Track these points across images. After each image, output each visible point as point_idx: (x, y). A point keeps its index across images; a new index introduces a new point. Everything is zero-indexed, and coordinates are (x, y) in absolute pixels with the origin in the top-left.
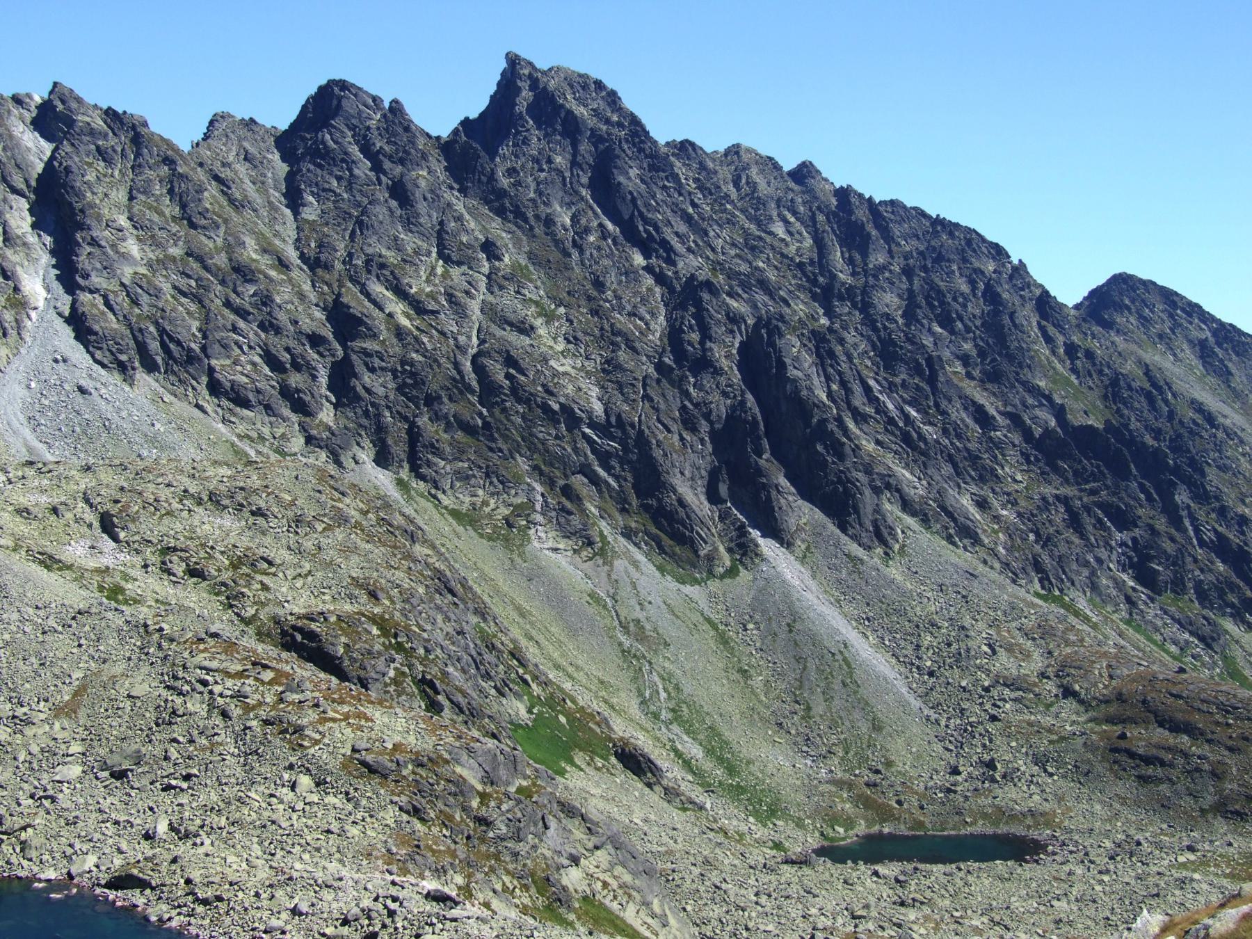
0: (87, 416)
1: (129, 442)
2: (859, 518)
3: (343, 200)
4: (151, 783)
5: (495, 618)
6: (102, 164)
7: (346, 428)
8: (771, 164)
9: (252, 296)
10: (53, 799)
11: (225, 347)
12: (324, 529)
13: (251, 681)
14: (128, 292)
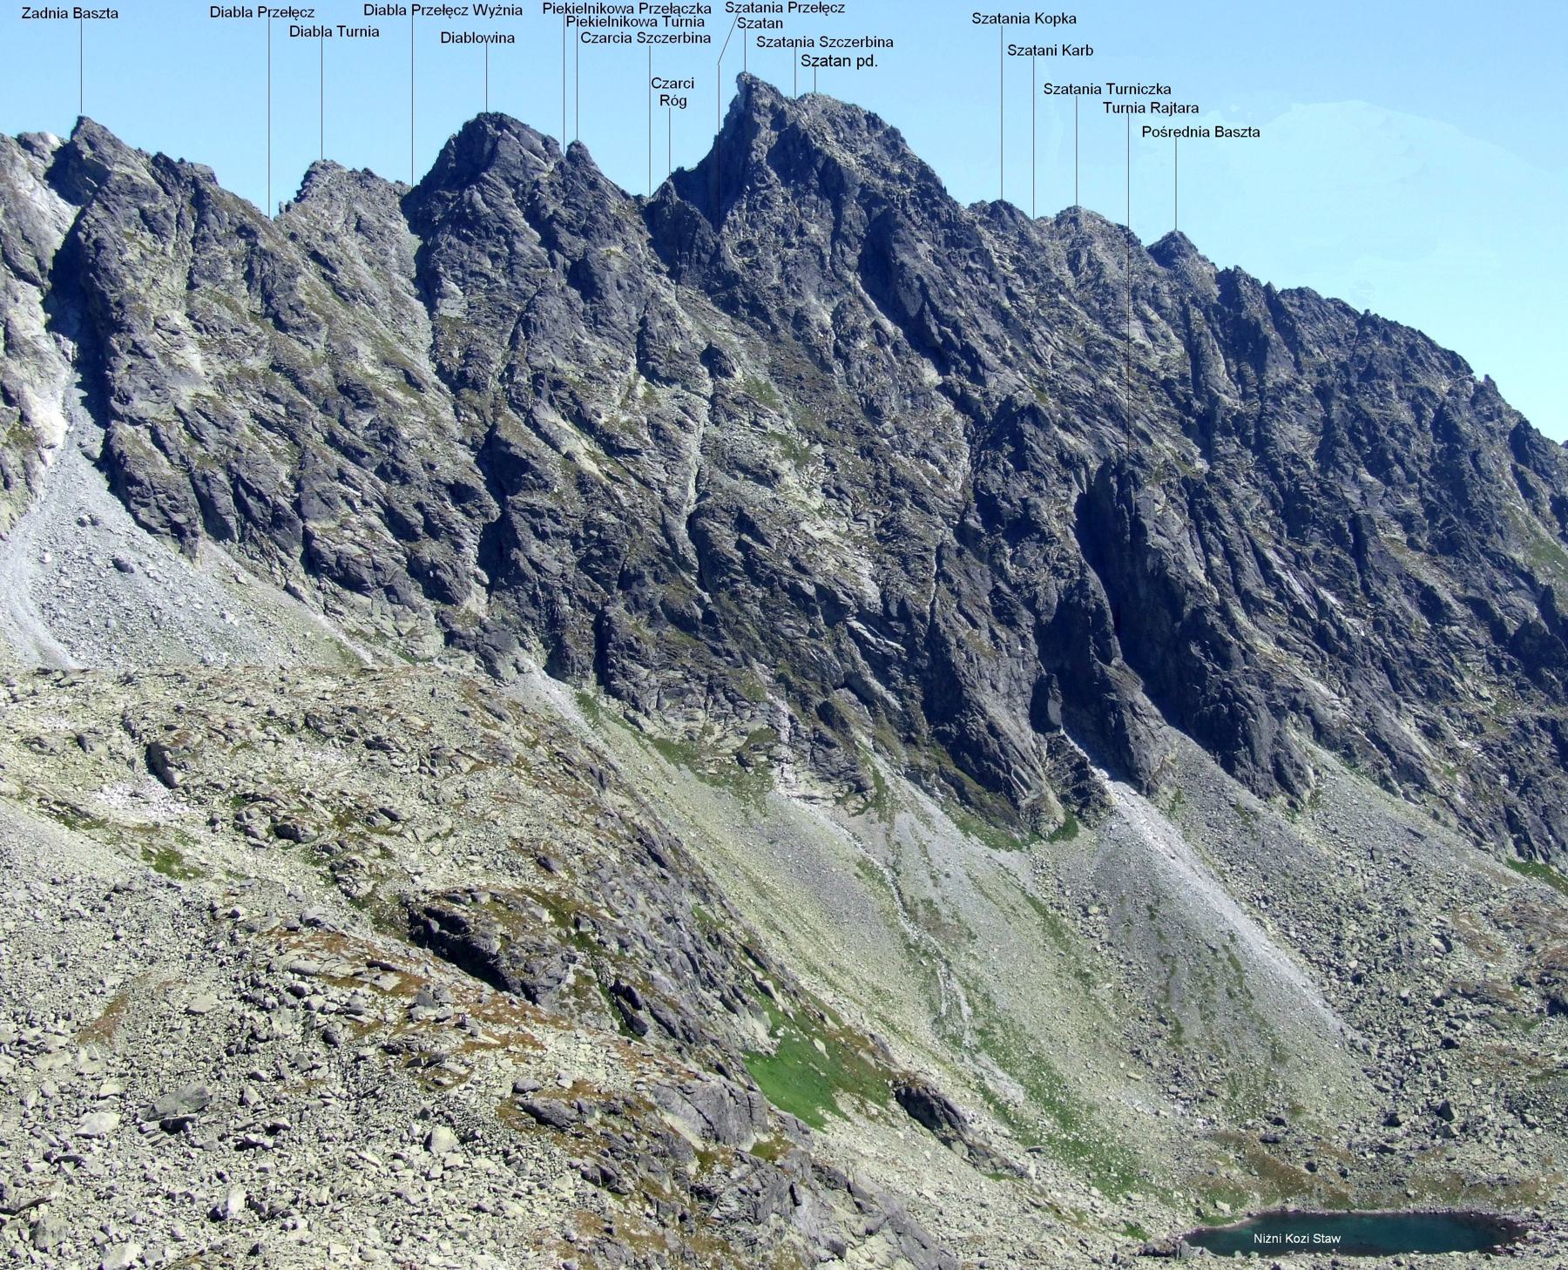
0: (126, 604)
1: (188, 642)
2: (1252, 752)
3: (500, 288)
4: (220, 1139)
7: (504, 620)
9: (368, 428)
10: (77, 1162)
11: (328, 502)
12: (473, 768)
13: (365, 990)
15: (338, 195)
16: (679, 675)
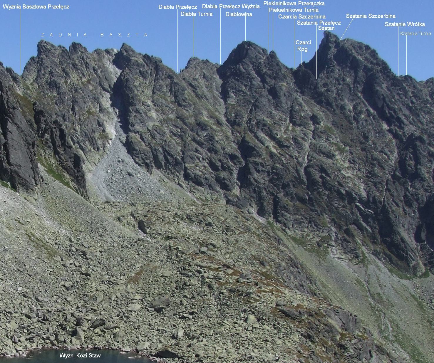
0: (131, 185)
1: (149, 198)
3: (247, 95)
4: (174, 315)
5: (315, 283)
6: (142, 78)
10: (128, 318)
11: (192, 158)
12: (239, 233)
13: (222, 273)
15: (198, 67)
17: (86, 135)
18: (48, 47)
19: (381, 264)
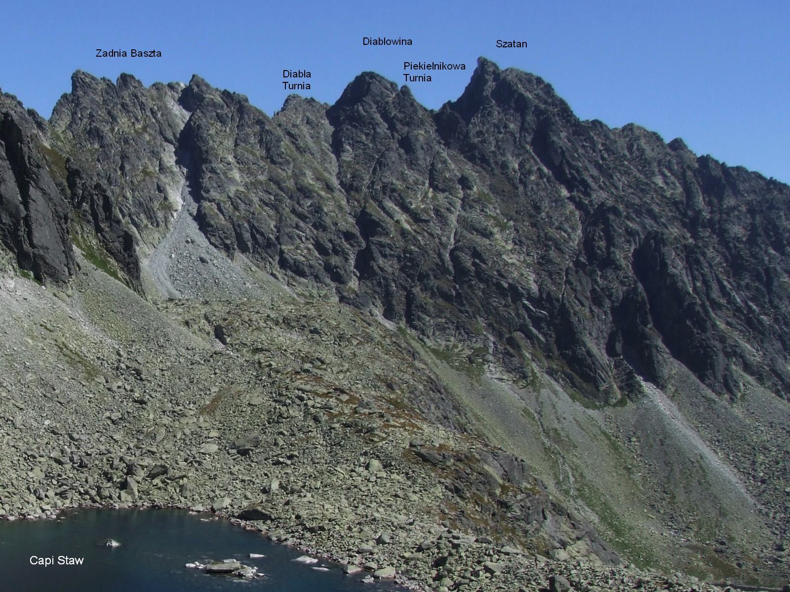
0: (205, 276)
1: (230, 293)
2: (714, 372)
3: (369, 148)
4: (265, 460)
5: (465, 414)
6: (219, 124)
7: (366, 292)
8: (655, 138)
9: (309, 206)
10: (200, 463)
11: (291, 238)
12: (358, 344)
14: (232, 202)
16: (444, 320)
17: (141, 204)
18: (87, 80)
19: (558, 388)
